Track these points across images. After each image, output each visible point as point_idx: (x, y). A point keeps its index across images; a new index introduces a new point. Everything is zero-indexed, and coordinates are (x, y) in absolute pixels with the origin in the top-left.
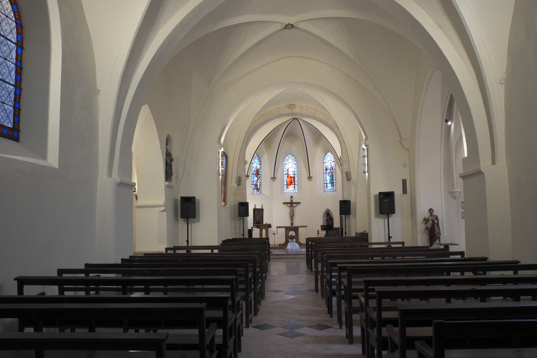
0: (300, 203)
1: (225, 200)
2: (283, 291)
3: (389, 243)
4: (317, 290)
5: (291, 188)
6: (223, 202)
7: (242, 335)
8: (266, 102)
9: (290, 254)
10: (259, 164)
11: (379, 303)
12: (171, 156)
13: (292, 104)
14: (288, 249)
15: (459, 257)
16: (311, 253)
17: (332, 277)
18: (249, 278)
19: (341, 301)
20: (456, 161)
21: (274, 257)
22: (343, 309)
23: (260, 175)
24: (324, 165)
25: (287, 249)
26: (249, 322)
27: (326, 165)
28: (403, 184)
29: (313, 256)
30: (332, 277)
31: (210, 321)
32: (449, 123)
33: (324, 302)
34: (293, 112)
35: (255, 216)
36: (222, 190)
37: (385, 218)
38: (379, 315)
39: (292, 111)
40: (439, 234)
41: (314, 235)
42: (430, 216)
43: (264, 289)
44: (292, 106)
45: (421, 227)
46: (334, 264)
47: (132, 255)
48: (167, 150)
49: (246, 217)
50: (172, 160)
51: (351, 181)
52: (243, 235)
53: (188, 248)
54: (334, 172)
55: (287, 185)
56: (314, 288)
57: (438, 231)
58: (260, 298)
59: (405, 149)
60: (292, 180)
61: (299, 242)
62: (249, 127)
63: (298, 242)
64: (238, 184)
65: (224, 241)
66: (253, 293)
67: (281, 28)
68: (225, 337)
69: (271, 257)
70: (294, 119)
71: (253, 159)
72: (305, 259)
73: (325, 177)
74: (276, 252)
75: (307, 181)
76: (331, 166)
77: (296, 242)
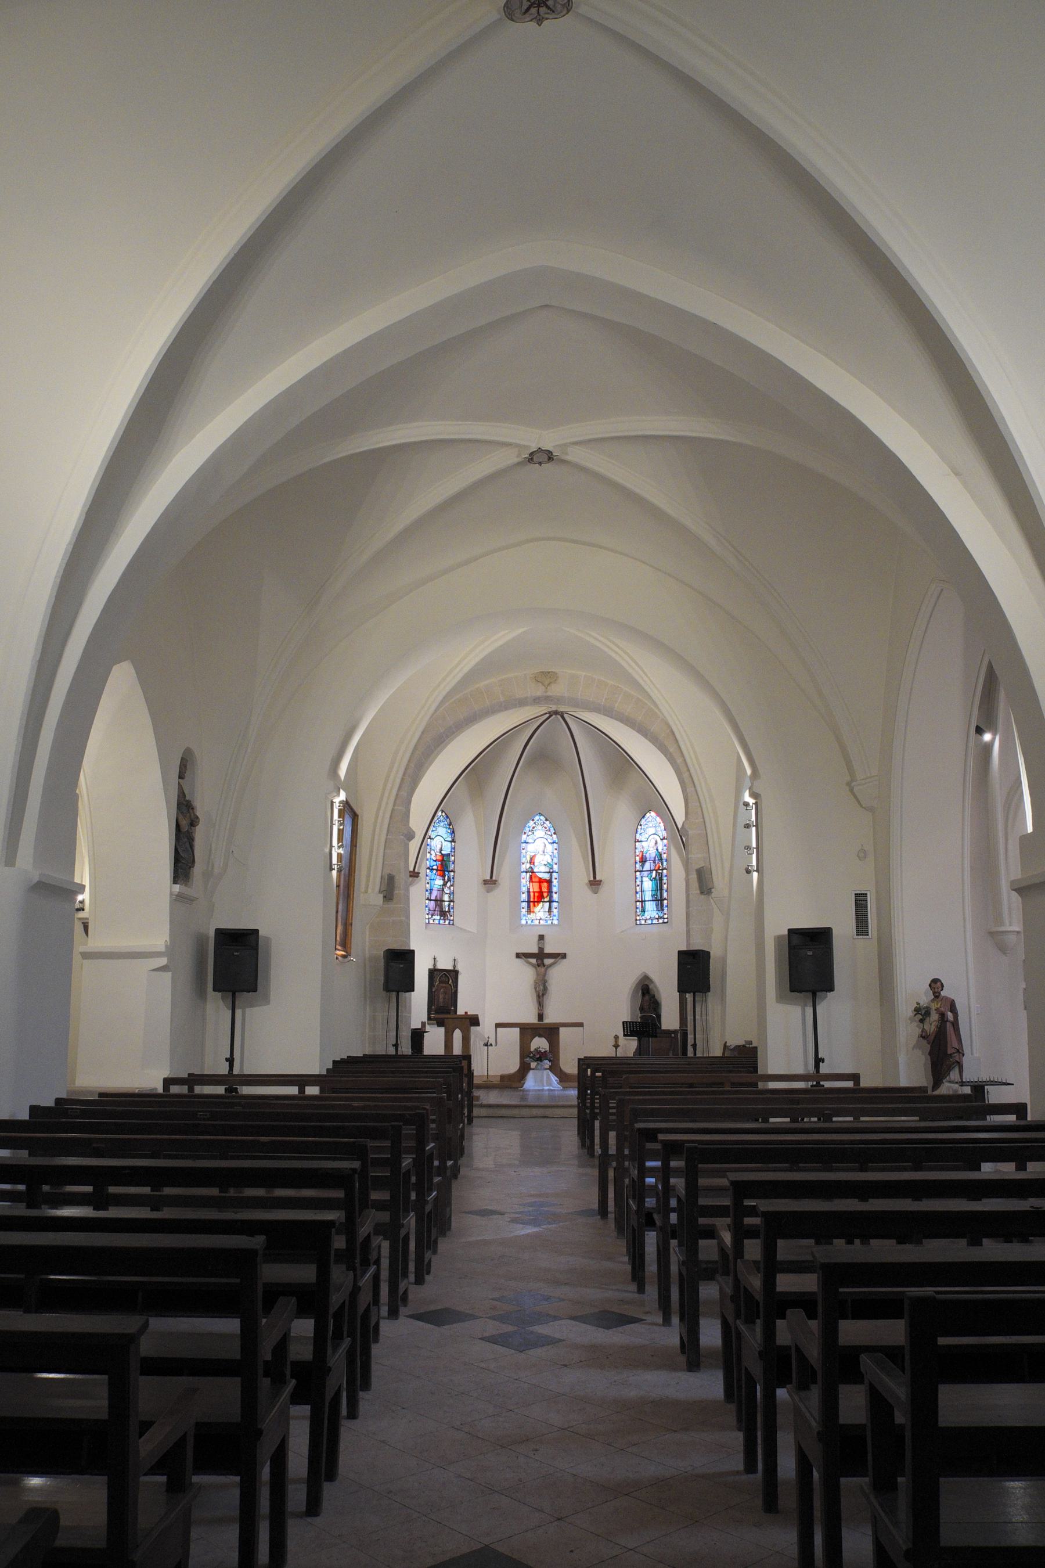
0: (564, 956)
1: (345, 943)
2: (504, 1214)
3: (817, 1076)
4: (603, 1211)
5: (540, 911)
6: (338, 947)
7: (376, 1341)
8: (473, 663)
9: (532, 1104)
10: (450, 839)
11: (770, 1250)
12: (191, 811)
13: (549, 672)
14: (529, 1091)
15: (1011, 1118)
16: (593, 1103)
17: (643, 1172)
18: (403, 1171)
19: (669, 1244)
20: (1006, 844)
21: (484, 1112)
22: (674, 1268)
23: (452, 871)
24: (636, 848)
25: (523, 1091)
26: (400, 1303)
27: (643, 847)
28: (857, 906)
29: (597, 1111)
30: (643, 1172)
31: (274, 1294)
32: (987, 737)
33: (621, 1247)
34: (549, 694)
35: (434, 990)
36: (337, 912)
37: (805, 1005)
38: (769, 1282)
39: (546, 692)
40: (960, 1051)
41: (605, 1050)
42: (932, 1001)
43: (449, 1204)
44: (547, 677)
45: (907, 1032)
46: (650, 1135)
47: (64, 1096)
48: (181, 794)
49: (407, 994)
50: (194, 822)
51: (713, 895)
52: (396, 1046)
53: (232, 1080)
54: (665, 869)
55: (529, 902)
56: (596, 1206)
57: (956, 1046)
58: (434, 1231)
59: (863, 808)
60: (545, 889)
61: (561, 1070)
62: (423, 733)
63: (555, 1068)
64: (385, 897)
65: (337, 1061)
66: (412, 1214)
67: (519, 460)
68: (319, 1340)
69: (476, 1112)
70: (551, 714)
71: (432, 827)
72: (575, 1122)
73: (638, 883)
74: (492, 1097)
75: (587, 892)
76: (657, 850)
77: (551, 1069)
